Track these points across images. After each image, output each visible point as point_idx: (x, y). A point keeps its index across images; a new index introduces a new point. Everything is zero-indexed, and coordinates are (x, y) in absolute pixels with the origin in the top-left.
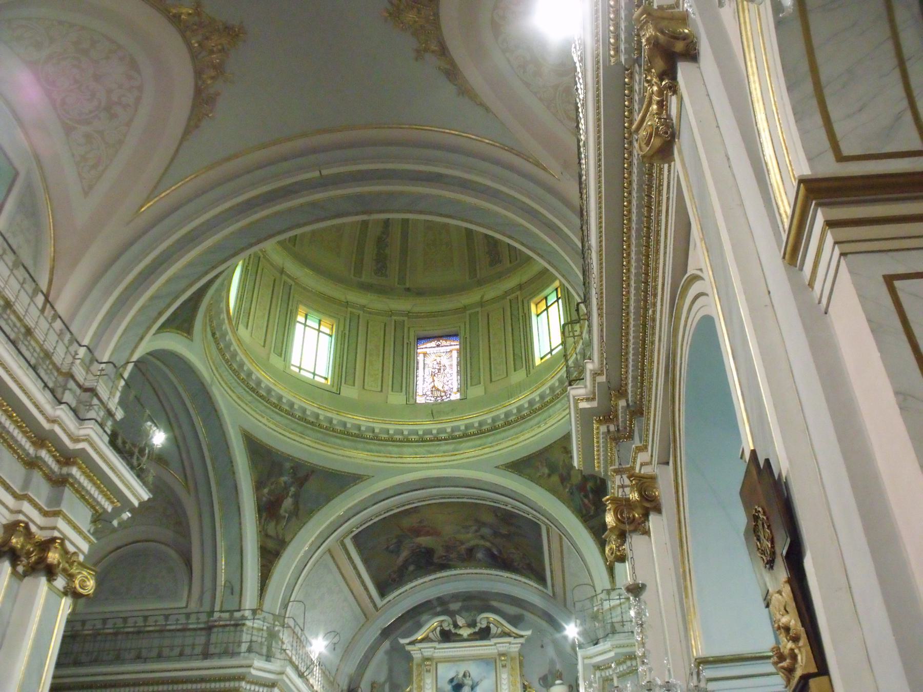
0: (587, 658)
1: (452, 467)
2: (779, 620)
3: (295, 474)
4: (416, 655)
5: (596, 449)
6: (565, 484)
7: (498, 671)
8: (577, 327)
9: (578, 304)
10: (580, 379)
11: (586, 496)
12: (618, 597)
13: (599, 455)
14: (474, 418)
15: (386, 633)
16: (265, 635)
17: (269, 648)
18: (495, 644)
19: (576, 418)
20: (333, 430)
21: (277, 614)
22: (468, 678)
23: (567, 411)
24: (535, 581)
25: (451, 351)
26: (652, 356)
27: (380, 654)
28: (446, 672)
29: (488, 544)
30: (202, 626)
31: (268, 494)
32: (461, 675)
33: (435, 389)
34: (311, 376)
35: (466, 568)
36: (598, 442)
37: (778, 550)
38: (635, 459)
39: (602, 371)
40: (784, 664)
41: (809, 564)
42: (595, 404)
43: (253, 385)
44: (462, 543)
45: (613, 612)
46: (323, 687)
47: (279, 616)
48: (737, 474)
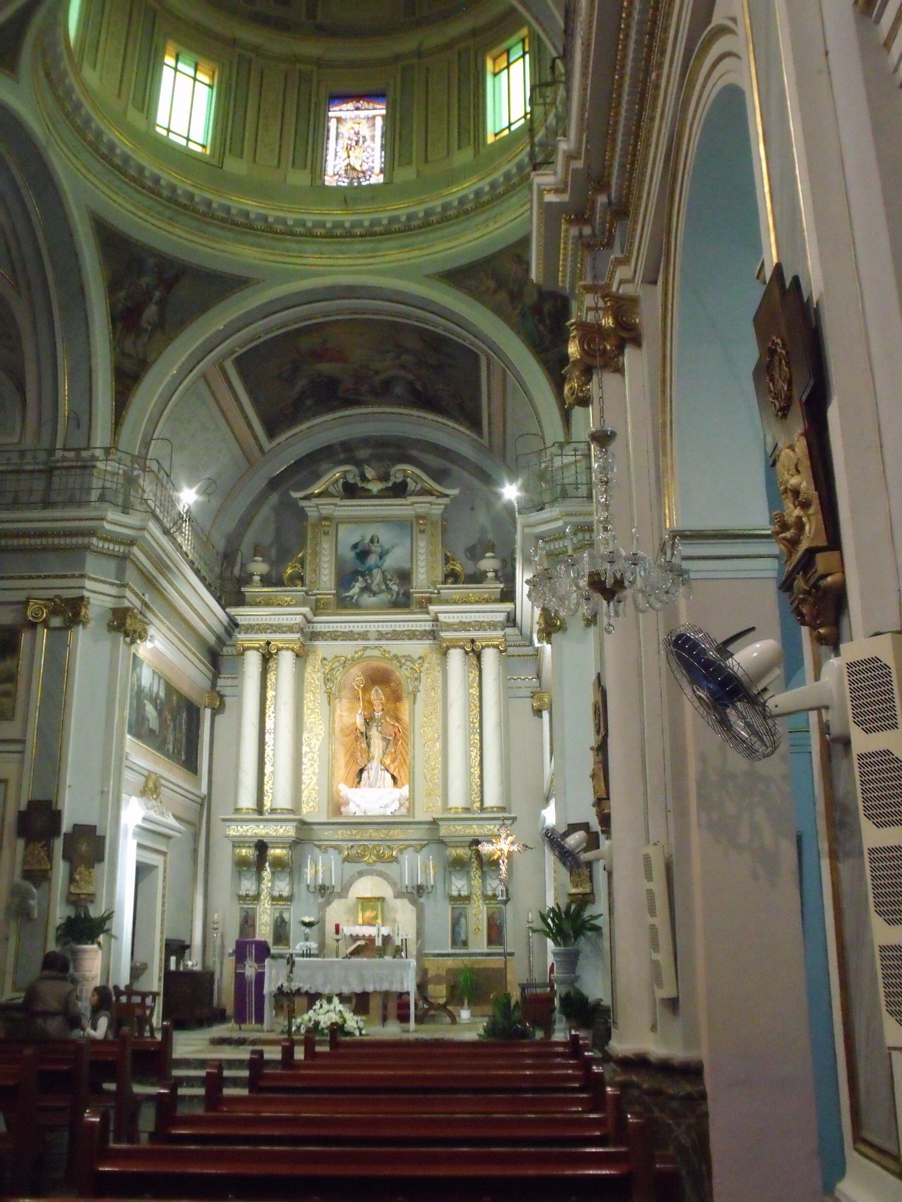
0: (528, 526)
1: (369, 272)
2: (787, 481)
4: (312, 513)
5: (561, 257)
7: (414, 538)
8: (549, 92)
9: (554, 61)
10: (548, 162)
11: (542, 321)
12: (573, 453)
13: (564, 266)
14: (400, 209)
15: (275, 483)
16: (121, 480)
17: (127, 497)
18: (412, 504)
19: (539, 214)
20: (213, 217)
21: (136, 453)
22: (376, 544)
23: (527, 206)
24: (469, 428)
25: (374, 117)
26: (648, 138)
27: (266, 511)
28: (349, 536)
29: (410, 376)
30: (41, 467)
32: (367, 540)
33: (350, 168)
34: (183, 142)
35: (380, 405)
36: (565, 249)
37: (796, 393)
38: (613, 273)
39: (579, 153)
40: (788, 534)
41: (833, 414)
42: (565, 198)
43: (105, 150)
44: (377, 373)
45: (565, 470)
46: (194, 548)
47: (138, 457)
48: (755, 295)
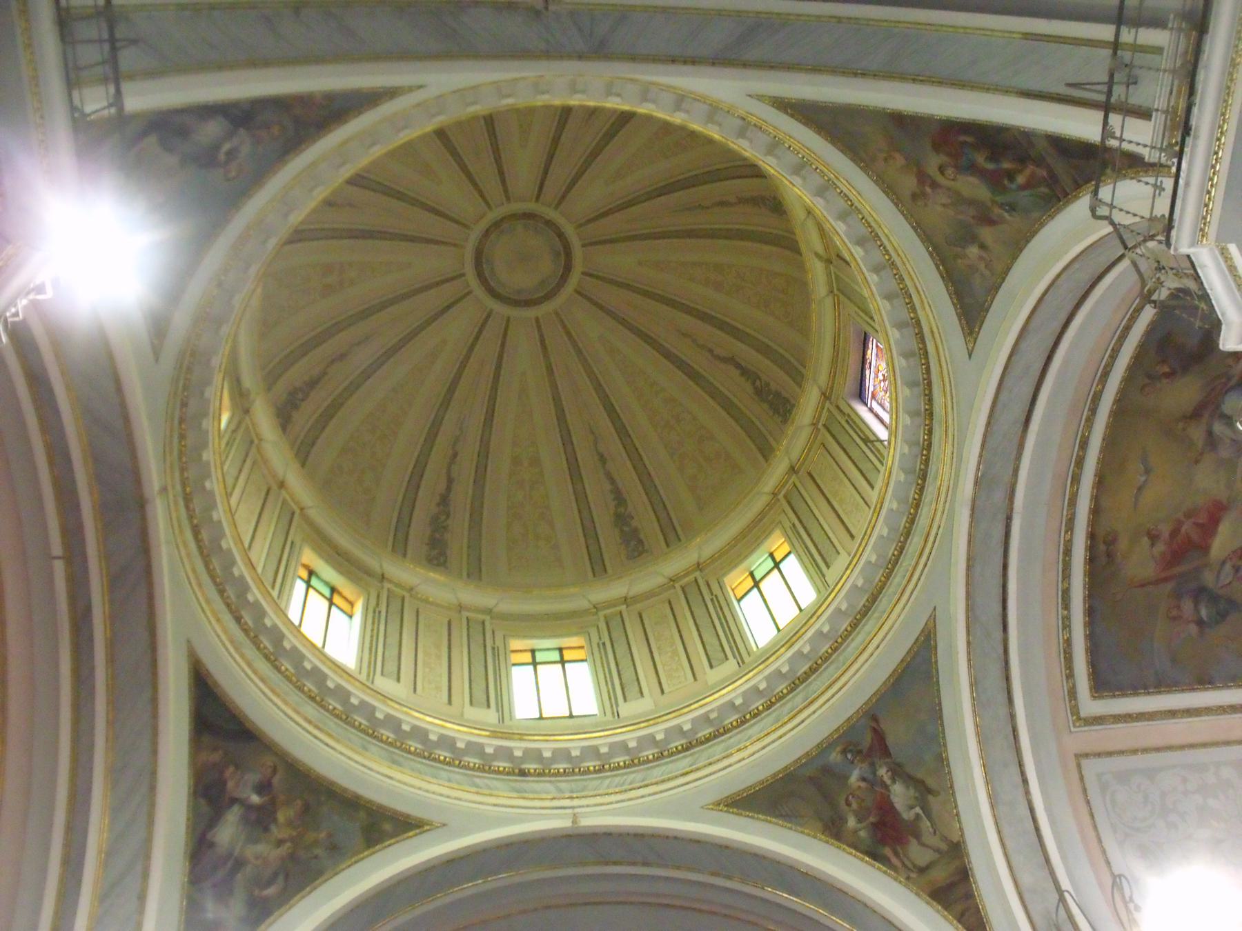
3: (860, 752)
6: (995, 218)
11: (1011, 176)
31: (860, 821)
